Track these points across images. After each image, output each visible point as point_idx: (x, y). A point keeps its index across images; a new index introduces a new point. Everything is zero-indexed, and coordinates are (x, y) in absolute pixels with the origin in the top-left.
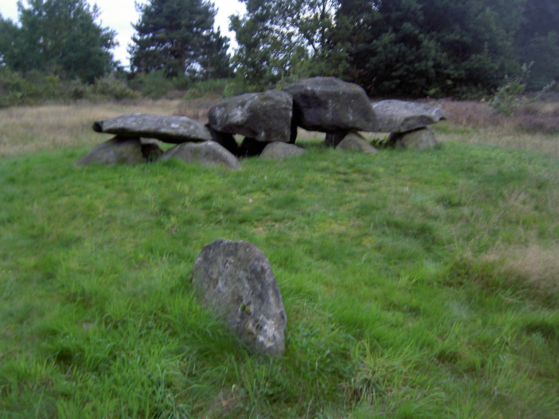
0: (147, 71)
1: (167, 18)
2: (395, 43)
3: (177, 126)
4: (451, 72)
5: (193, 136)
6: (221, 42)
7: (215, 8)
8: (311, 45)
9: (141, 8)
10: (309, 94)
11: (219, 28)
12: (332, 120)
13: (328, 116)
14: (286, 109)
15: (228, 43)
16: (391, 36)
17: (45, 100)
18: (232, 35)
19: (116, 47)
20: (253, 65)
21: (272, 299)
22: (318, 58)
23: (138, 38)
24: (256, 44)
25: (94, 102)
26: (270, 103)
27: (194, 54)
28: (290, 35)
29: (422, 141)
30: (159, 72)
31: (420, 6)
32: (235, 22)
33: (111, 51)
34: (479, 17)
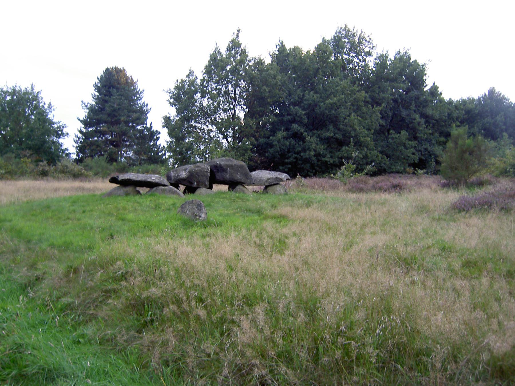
0: (92, 156)
1: (109, 115)
2: (286, 138)
3: (155, 179)
4: (328, 160)
5: (162, 183)
6: (153, 135)
7: (149, 107)
8: (225, 139)
9: (86, 106)
10: (218, 165)
11: (151, 124)
12: (229, 178)
13: (228, 176)
14: (207, 172)
15: (159, 136)
16: (283, 134)
17: (19, 176)
18: (165, 131)
19: (66, 137)
20: (181, 153)
21: (203, 209)
22: (232, 148)
23: (84, 130)
24: (183, 138)
25: (58, 179)
26: (199, 169)
27: (130, 144)
28: (209, 131)
29: (277, 190)
30: (101, 157)
31: (303, 113)
32: (167, 120)
33: (61, 141)
34: (346, 121)
